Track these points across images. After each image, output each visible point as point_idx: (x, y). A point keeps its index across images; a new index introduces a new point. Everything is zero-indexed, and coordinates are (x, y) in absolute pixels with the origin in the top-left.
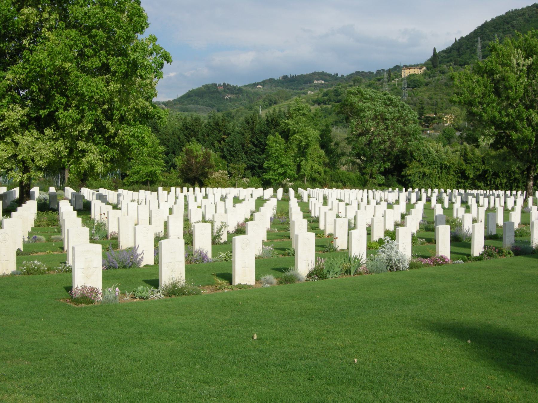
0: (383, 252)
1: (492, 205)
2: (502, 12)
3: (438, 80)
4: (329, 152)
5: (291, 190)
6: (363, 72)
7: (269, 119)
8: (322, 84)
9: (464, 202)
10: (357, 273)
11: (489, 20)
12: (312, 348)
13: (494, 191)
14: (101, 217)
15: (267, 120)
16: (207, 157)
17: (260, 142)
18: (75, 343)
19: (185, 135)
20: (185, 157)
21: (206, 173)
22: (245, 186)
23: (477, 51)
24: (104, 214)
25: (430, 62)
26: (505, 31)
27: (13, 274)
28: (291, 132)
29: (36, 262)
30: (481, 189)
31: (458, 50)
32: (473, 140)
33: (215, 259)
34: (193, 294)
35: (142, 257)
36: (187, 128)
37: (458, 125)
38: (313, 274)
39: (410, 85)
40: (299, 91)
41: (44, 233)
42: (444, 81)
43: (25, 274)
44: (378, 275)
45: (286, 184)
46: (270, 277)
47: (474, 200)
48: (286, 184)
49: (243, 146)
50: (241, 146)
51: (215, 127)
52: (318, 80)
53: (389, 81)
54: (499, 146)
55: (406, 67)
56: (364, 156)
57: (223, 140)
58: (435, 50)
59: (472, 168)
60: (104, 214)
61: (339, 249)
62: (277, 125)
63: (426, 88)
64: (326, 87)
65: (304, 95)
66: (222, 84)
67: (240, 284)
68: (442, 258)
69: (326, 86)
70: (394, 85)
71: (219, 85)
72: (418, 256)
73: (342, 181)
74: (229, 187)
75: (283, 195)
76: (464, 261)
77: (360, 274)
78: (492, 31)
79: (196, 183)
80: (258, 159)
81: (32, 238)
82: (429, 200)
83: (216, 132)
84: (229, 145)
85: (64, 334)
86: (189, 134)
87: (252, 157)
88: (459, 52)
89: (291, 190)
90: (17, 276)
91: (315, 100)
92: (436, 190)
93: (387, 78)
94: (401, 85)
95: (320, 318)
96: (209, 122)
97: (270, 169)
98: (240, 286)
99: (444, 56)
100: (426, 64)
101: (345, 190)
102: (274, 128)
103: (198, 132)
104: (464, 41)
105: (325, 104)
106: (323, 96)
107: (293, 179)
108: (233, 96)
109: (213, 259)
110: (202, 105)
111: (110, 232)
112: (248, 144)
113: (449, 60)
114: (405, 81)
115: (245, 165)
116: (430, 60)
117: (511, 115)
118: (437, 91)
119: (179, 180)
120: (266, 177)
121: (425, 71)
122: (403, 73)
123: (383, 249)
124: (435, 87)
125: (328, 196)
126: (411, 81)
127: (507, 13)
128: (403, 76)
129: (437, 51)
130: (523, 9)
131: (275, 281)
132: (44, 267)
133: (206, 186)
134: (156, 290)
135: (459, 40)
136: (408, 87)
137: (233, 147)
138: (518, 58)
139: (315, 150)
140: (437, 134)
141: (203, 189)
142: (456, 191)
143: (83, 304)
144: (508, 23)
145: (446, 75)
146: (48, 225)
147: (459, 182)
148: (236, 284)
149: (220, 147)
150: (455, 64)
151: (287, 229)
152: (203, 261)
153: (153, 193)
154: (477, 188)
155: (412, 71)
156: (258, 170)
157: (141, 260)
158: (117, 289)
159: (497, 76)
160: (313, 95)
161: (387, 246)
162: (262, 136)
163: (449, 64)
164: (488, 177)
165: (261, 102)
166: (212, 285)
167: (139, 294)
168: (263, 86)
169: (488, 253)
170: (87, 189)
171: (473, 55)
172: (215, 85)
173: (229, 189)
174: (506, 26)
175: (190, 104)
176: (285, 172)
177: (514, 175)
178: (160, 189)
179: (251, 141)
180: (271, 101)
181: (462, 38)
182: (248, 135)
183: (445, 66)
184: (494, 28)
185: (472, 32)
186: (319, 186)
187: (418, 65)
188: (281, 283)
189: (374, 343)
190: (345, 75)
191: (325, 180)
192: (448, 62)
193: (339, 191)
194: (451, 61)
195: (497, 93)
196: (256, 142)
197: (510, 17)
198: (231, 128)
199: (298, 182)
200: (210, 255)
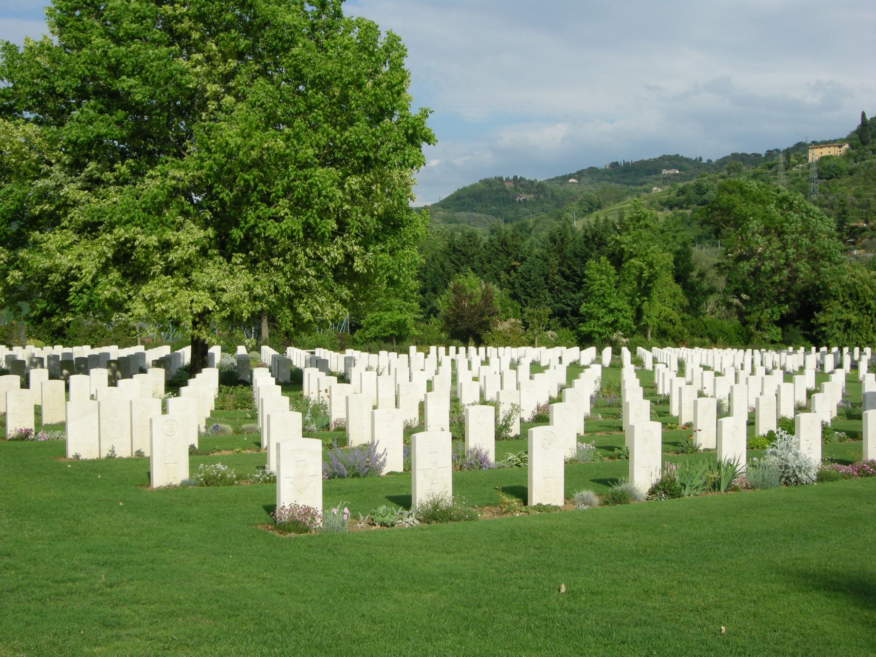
6: (743, 154)
7: (589, 234)
10: (731, 488)
15: (585, 237)
16: (487, 297)
17: (574, 271)
19: (452, 262)
22: (550, 345)
25: (857, 136)
27: (184, 484)
28: (626, 256)
36: (455, 250)
38: (659, 489)
39: (822, 174)
41: (230, 420)
43: (202, 485)
45: (616, 341)
48: (616, 341)
49: (546, 279)
50: (543, 278)
51: (500, 248)
52: (668, 168)
53: (787, 169)
55: (816, 144)
56: (746, 293)
57: (514, 268)
58: (863, 115)
60: (326, 391)
61: (701, 448)
65: (646, 194)
66: (511, 178)
69: (682, 178)
70: (797, 175)
71: (507, 179)
74: (524, 345)
77: (736, 489)
79: (471, 339)
80: (571, 300)
83: (502, 256)
84: (523, 277)
85: (264, 579)
86: (459, 260)
87: (561, 296)
90: (191, 487)
91: (664, 201)
93: (784, 164)
94: (807, 174)
95: (667, 561)
97: (591, 316)
98: (540, 508)
100: (848, 139)
101: (715, 349)
102: (598, 249)
103: (473, 256)
105: (681, 208)
106: (678, 195)
108: (529, 197)
112: (554, 275)
115: (549, 310)
116: (857, 132)
118: (869, 184)
121: (847, 150)
122: (810, 155)
123: (774, 449)
128: (810, 160)
129: (868, 118)
131: (596, 500)
132: (232, 474)
133: (487, 345)
134: (406, 513)
136: (819, 178)
141: (482, 349)
143: (293, 534)
146: (236, 408)
148: (534, 504)
149: (508, 280)
151: (618, 416)
152: (481, 467)
153: (401, 355)
155: (826, 151)
156: (571, 318)
157: (383, 464)
158: (346, 510)
162: (578, 261)
165: (574, 206)
166: (495, 505)
167: (380, 519)
168: (579, 179)
170: (296, 349)
172: (501, 179)
175: (459, 211)
176: (616, 321)
178: (413, 349)
179: (559, 271)
182: (554, 261)
187: (835, 141)
188: (607, 503)
199: (638, 338)
200: (492, 458)
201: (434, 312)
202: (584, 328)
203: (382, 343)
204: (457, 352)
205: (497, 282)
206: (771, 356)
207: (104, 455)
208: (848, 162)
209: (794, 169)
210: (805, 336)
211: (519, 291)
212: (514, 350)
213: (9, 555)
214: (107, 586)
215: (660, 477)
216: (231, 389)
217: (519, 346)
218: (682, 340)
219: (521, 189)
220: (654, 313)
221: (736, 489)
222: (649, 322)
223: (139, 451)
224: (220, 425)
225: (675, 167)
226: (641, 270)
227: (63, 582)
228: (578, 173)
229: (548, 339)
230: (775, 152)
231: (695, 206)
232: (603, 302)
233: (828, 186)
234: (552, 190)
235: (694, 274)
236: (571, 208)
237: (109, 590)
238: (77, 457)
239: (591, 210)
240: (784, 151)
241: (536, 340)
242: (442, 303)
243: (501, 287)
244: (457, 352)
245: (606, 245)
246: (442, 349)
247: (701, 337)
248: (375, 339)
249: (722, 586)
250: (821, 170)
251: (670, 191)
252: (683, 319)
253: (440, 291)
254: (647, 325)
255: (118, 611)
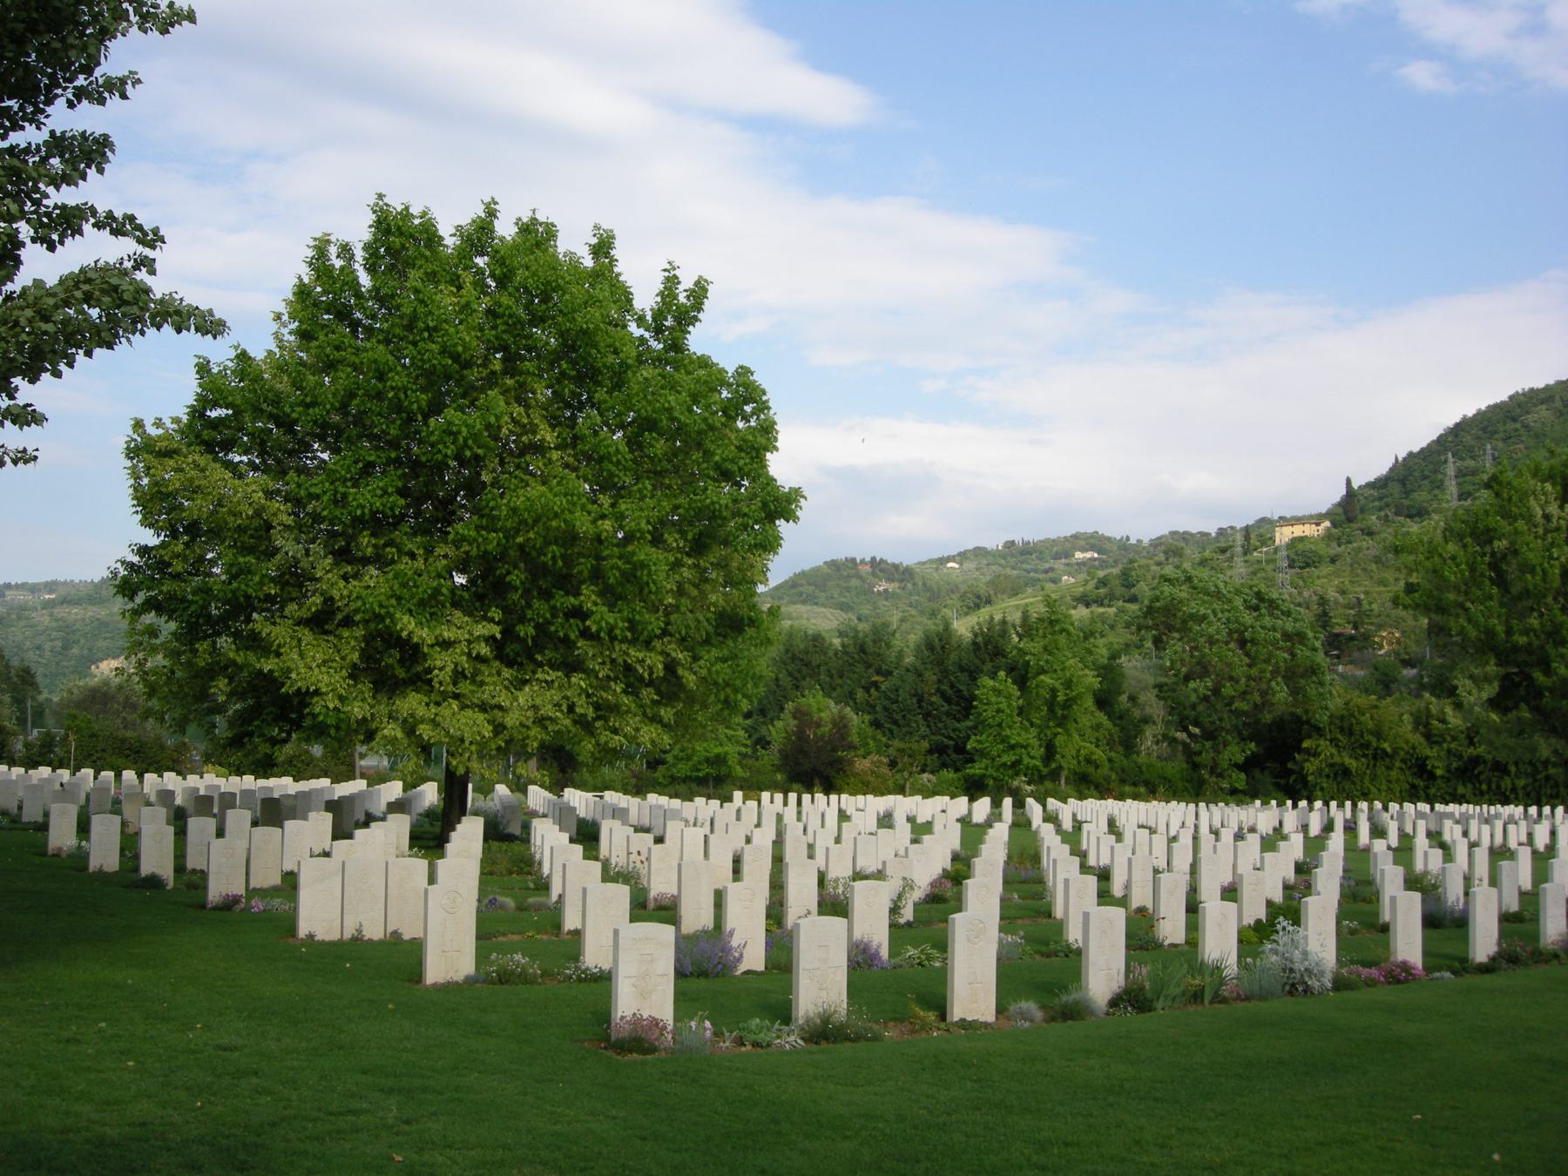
0: (1276, 952)
1: (1499, 840)
2: (1501, 395)
3: (1360, 549)
4: (1118, 717)
5: (1030, 801)
6: (1185, 533)
7: (980, 639)
8: (1093, 559)
9: (1435, 837)
10: (1218, 999)
11: (1470, 414)
12: (1152, 1165)
13: (1499, 806)
14: (628, 858)
15: (974, 643)
16: (841, 725)
17: (960, 691)
18: (645, 1139)
19: (790, 674)
20: (793, 723)
21: (840, 760)
22: (928, 793)
23: (1447, 483)
24: (639, 853)
25: (1340, 510)
26: (1509, 438)
27: (469, 981)
28: (1032, 671)
29: (518, 957)
30: (1468, 803)
31: (1403, 482)
32: (1444, 689)
33: (897, 960)
34: (868, 1040)
35: (741, 955)
36: (794, 658)
37: (1407, 653)
38: (1122, 999)
39: (1293, 561)
40: (1041, 576)
41: (506, 890)
42: (1374, 552)
43: (494, 983)
44: (1262, 1004)
45: (1018, 789)
46: (1029, 1006)
47: (1458, 829)
48: (1018, 789)
49: (920, 701)
50: (915, 700)
51: (856, 656)
52: (1083, 550)
53: (1245, 554)
54: (1510, 704)
55: (1285, 521)
56: (1196, 724)
57: (876, 685)
58: (1349, 481)
59: (1443, 754)
60: (639, 853)
61: (1166, 943)
62: (998, 652)
63: (1331, 568)
64: (1101, 567)
65: (1052, 585)
66: (868, 559)
67: (963, 1020)
68: (1405, 967)
69: (1103, 564)
70: (1259, 562)
71: (862, 561)
72: (1352, 962)
73: (1146, 783)
74: (890, 793)
75: (1014, 813)
76: (1454, 973)
77: (1224, 1001)
78: (1479, 438)
79: (817, 781)
80: (954, 730)
81: (486, 901)
82: (1351, 828)
83: (859, 668)
84: (888, 698)
85: (614, 1118)
86: (799, 671)
87: (940, 725)
88: (1404, 485)
89: (1030, 801)
90: (478, 985)
91: (1078, 595)
92: (1363, 805)
93: (1243, 547)
94: (1274, 561)
95: (1156, 1100)
96: (843, 646)
97: (983, 753)
98: (964, 1024)
99: (1372, 495)
100: (1328, 515)
101: (1155, 803)
102: (992, 660)
103: (819, 666)
104: (1416, 460)
105: (1102, 605)
106: (1097, 588)
107: (1036, 778)
108: (892, 587)
109: (893, 961)
110: (823, 605)
111: (653, 894)
112: (931, 695)
113: (1382, 504)
114: (1285, 553)
115: (925, 745)
116: (1339, 504)
117: (1535, 631)
118: (1358, 575)
119: (779, 777)
120: (971, 771)
121: (1327, 529)
122: (1278, 536)
123: (1274, 945)
124: (1351, 566)
125: (1117, 818)
126: (1297, 554)
127: (1511, 398)
128: (1277, 542)
129: (1355, 485)
130: (1547, 388)
131: (1039, 1015)
132: (535, 970)
133: (839, 792)
134: (786, 1028)
135: (1404, 459)
136: (1291, 566)
137: (897, 701)
138: (1546, 501)
139: (1088, 715)
140: (1360, 673)
141: (834, 798)
142: (1409, 807)
143: (635, 1055)
144: (1514, 420)
145: (1378, 538)
146: (510, 873)
147: (1413, 786)
148: (956, 1019)
149: (868, 702)
150: (1397, 514)
151: (1040, 896)
152: (870, 966)
153: (710, 801)
154: (1460, 800)
155: (1298, 531)
156: (954, 756)
157: (739, 959)
158: (708, 1024)
159: (1500, 545)
160: (1074, 585)
161: (1282, 938)
162: (964, 677)
163: (1382, 514)
164: (1480, 773)
165: (954, 600)
166: (902, 1021)
167: (753, 1037)
168: (961, 564)
169: (1506, 959)
170: (578, 793)
171: (1436, 492)
172: (853, 560)
173: (891, 798)
174: (1510, 426)
175: (795, 603)
176: (1018, 763)
177: (1546, 768)
178: (738, 795)
179: (938, 690)
180: (978, 597)
181: (1411, 454)
182: (931, 676)
183: (1374, 518)
184: (1484, 430)
185: (1433, 442)
186: (1095, 793)
187: (1311, 517)
188: (1053, 1019)
189: (1286, 1156)
190: (1146, 541)
191: (1107, 779)
192: (1380, 509)
193: (1143, 805)
194: (1387, 505)
195: (1501, 581)
196: (950, 692)
197: (1519, 405)
198: (893, 659)
199: (1048, 784)
200: (884, 953)
201: (763, 743)
202: (975, 770)
203: (693, 786)
204: (785, 804)
205: (851, 703)
206: (1234, 815)
207: (347, 935)
208: (1328, 545)
209: (1255, 554)
210: (1277, 786)
211: (881, 716)
212: (879, 799)
213: (256, 1073)
214: (404, 1122)
215: (1122, 983)
216: (504, 847)
217: (882, 794)
218: (1108, 789)
219: (881, 574)
220: (1070, 751)
221: (1224, 1001)
222: (1064, 764)
223: (395, 933)
224: (498, 897)
225: (1092, 548)
226: (1054, 691)
227: (342, 1114)
228: (960, 554)
229: (923, 785)
230: (1229, 531)
231: (1120, 603)
232: (999, 734)
233: (1302, 578)
234: (923, 578)
235: (1123, 698)
236: (949, 602)
237: (406, 1128)
238: (311, 936)
239: (978, 607)
240: (1241, 529)
241: (908, 786)
242: (780, 730)
243: (856, 710)
244: (785, 804)
245: (1004, 656)
246: (779, 797)
247: (1135, 784)
248: (686, 780)
249: (1237, 1135)
250: (1292, 556)
251: (1087, 582)
252: (1110, 760)
253: (771, 714)
254: (1060, 768)
255: (426, 1157)
